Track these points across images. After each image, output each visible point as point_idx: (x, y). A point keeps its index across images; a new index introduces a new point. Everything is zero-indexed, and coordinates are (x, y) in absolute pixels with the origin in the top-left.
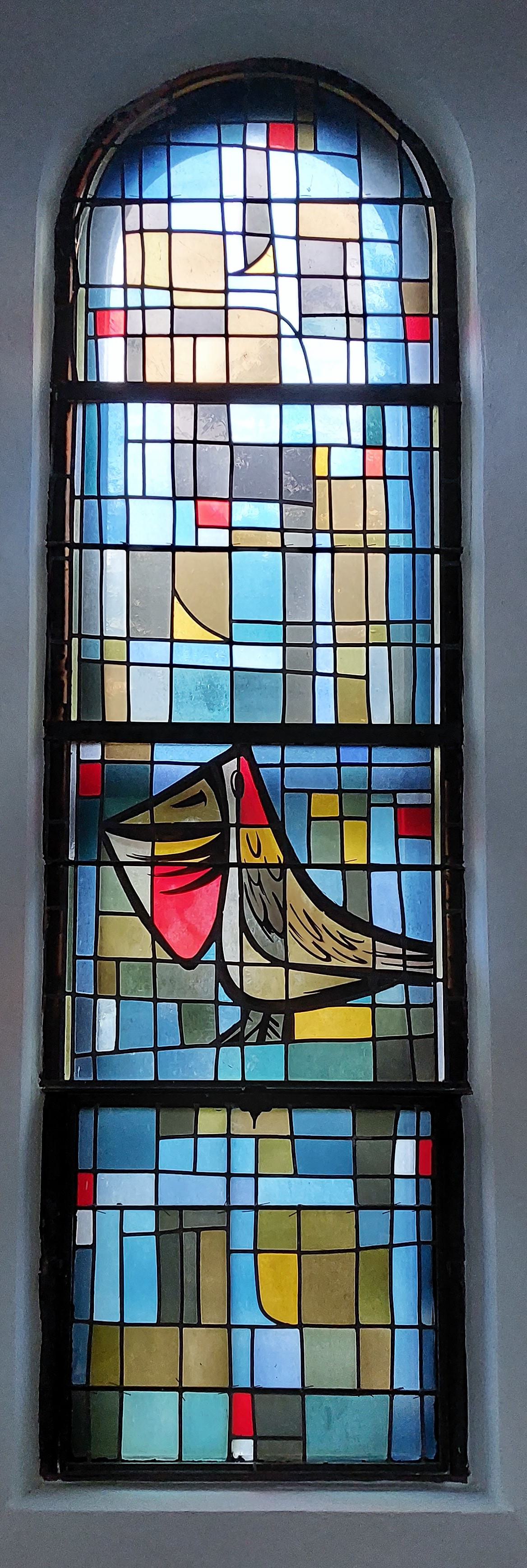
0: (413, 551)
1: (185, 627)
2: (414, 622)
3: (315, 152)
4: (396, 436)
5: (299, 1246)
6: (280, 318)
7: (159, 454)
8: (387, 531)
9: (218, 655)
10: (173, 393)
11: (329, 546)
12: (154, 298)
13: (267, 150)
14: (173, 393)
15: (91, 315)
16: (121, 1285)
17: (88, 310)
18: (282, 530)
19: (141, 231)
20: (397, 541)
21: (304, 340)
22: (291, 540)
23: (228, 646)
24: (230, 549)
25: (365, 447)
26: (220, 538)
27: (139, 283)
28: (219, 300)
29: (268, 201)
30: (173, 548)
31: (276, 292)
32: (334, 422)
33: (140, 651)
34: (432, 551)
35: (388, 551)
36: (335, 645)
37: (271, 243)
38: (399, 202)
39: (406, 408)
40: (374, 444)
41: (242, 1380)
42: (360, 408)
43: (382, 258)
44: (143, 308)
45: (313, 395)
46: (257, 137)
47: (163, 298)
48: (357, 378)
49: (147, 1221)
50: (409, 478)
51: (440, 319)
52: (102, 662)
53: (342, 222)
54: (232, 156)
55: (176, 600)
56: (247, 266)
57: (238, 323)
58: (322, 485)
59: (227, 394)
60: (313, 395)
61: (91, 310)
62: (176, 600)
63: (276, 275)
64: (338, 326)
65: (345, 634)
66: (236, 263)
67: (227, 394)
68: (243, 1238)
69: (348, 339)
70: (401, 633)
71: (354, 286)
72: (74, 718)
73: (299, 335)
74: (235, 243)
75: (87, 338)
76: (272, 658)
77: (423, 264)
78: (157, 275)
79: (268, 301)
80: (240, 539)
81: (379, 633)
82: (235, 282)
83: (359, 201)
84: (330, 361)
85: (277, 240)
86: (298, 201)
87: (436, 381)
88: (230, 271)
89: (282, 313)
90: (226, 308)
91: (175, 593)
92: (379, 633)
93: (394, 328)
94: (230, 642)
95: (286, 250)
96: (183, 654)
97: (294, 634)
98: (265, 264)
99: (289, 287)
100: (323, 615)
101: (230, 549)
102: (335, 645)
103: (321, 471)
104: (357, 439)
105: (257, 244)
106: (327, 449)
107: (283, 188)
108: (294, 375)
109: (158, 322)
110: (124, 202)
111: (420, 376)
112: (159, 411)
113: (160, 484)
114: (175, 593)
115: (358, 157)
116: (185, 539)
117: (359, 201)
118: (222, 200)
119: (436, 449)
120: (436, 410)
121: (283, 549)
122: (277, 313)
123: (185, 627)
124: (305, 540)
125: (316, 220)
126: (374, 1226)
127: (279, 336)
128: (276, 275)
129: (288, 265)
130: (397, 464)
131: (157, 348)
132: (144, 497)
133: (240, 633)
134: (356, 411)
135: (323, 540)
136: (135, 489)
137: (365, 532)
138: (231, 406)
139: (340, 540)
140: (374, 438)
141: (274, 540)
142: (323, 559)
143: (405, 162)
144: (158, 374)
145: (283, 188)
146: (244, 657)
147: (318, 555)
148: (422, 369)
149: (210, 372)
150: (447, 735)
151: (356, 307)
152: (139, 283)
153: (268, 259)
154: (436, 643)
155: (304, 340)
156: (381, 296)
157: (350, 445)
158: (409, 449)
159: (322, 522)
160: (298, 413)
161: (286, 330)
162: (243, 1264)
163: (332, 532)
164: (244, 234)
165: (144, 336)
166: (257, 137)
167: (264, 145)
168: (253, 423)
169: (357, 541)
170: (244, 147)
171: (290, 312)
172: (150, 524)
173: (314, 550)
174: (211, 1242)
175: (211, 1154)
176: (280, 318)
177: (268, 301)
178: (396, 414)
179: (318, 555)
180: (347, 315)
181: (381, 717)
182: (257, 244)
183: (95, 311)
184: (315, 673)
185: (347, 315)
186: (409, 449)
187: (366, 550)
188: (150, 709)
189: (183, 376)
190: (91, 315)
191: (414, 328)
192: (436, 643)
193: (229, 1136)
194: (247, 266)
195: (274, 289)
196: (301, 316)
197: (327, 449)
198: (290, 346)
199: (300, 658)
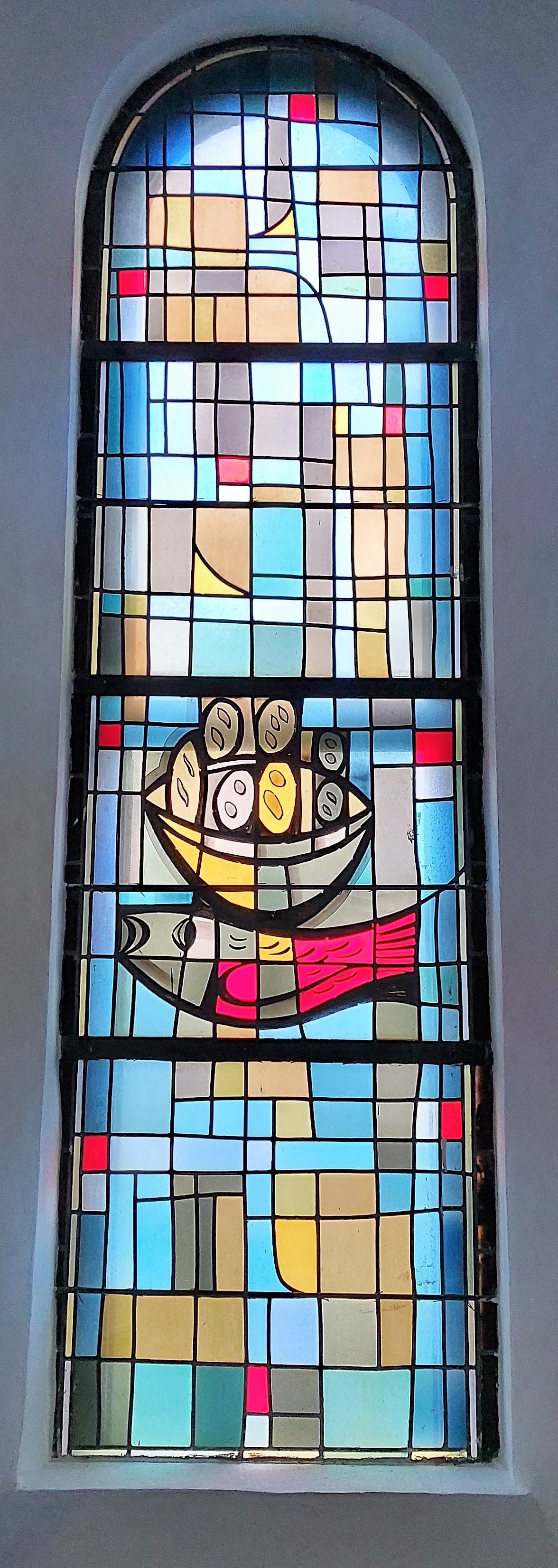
0: (433, 506)
1: (205, 581)
2: (434, 576)
3: (336, 121)
4: (416, 393)
5: (318, 1225)
6: (299, 278)
7: (180, 414)
8: (407, 488)
9: (239, 608)
10: (195, 352)
11: (349, 501)
12: (175, 258)
13: (289, 120)
14: (195, 352)
15: (114, 274)
16: (139, 1250)
17: (110, 270)
18: (302, 487)
19: (165, 401)
20: (415, 497)
21: (323, 299)
22: (313, 496)
23: (248, 600)
24: (251, 505)
25: (384, 405)
26: (241, 494)
27: (162, 397)
28: (239, 260)
29: (290, 169)
30: (194, 504)
31: (296, 253)
32: (351, 378)
33: (159, 605)
34: (450, 506)
35: (406, 506)
36: (355, 600)
37: (292, 208)
38: (420, 168)
39: (425, 365)
40: (392, 432)
41: (258, 1356)
42: (381, 366)
43: (401, 222)
44: (165, 268)
45: (333, 353)
46: (279, 106)
47: (185, 259)
48: (376, 337)
49: (161, 1186)
50: (429, 435)
51: (460, 285)
52: (123, 616)
53: (363, 186)
54: (255, 127)
55: (196, 555)
56: (268, 229)
57: (258, 282)
58: (342, 443)
59: (249, 352)
60: (333, 353)
61: (114, 270)
62: (196, 555)
63: (297, 237)
64: (358, 285)
65: (364, 589)
66: (257, 227)
67: (249, 352)
68: (258, 1203)
69: (368, 298)
70: (419, 587)
71: (374, 247)
72: (94, 671)
73: (319, 295)
74: (256, 208)
75: (110, 296)
76: (293, 612)
77: (440, 224)
78: (179, 236)
79: (289, 262)
80: (260, 495)
81: (398, 587)
82: (255, 244)
83: (380, 168)
84: (350, 323)
85: (297, 205)
86: (317, 169)
87: (454, 340)
88: (251, 233)
89: (302, 274)
90: (247, 268)
91: (195, 549)
92: (398, 587)
93: (414, 288)
94: (249, 595)
95: (306, 215)
96: (203, 607)
97: (315, 582)
98: (287, 227)
99: (309, 250)
100: (343, 570)
101: (251, 505)
102: (355, 600)
103: (342, 429)
104: (377, 398)
105: (277, 210)
106: (347, 407)
107: (303, 155)
108: (314, 334)
109: (179, 282)
110: (147, 169)
111: (439, 335)
112: (181, 373)
113: (181, 442)
114: (195, 549)
115: (379, 126)
116: (207, 494)
117: (380, 168)
118: (243, 168)
119: (457, 598)
120: (455, 368)
121: (304, 505)
122: (297, 274)
123: (205, 581)
124: (325, 497)
125: (335, 186)
126: (394, 1186)
127: (299, 295)
128: (297, 237)
129: (308, 229)
130: (416, 421)
131: (178, 308)
132: (166, 454)
133: (260, 586)
134: (377, 369)
135: (343, 497)
136: (157, 446)
137: (385, 489)
138: (253, 365)
139: (360, 497)
140: (394, 398)
141: (295, 496)
142: (343, 515)
143: (424, 131)
144: (178, 333)
145: (303, 155)
146: (264, 610)
147: (338, 511)
148: (441, 328)
149: (230, 333)
150: (466, 688)
151: (375, 267)
152: (162, 397)
153: (288, 223)
154: (452, 272)
155: (323, 299)
156: (401, 257)
157: (370, 404)
158: (429, 406)
159: (342, 480)
160: (317, 372)
161: (305, 289)
162: (259, 1230)
163: (352, 488)
164: (265, 199)
165: (165, 295)
166: (279, 106)
167: (286, 116)
168: (273, 380)
169: (377, 497)
170: (267, 117)
171: (310, 271)
172: (170, 480)
173: (334, 506)
174: (228, 1207)
175: (229, 1117)
176: (299, 278)
177: (289, 262)
178: (415, 372)
179: (338, 511)
180: (367, 274)
181: (401, 671)
182: (277, 210)
183: (118, 270)
184: (334, 627)
185: (367, 274)
186: (429, 406)
187: (386, 506)
188: (168, 661)
189: (204, 336)
190: (114, 274)
191: (432, 287)
192: (452, 272)
193: (243, 168)
194: (268, 229)
195: (294, 250)
196: (321, 275)
197: (347, 407)
198: (310, 305)
199: (320, 612)
